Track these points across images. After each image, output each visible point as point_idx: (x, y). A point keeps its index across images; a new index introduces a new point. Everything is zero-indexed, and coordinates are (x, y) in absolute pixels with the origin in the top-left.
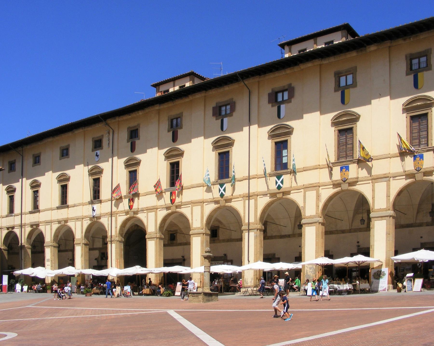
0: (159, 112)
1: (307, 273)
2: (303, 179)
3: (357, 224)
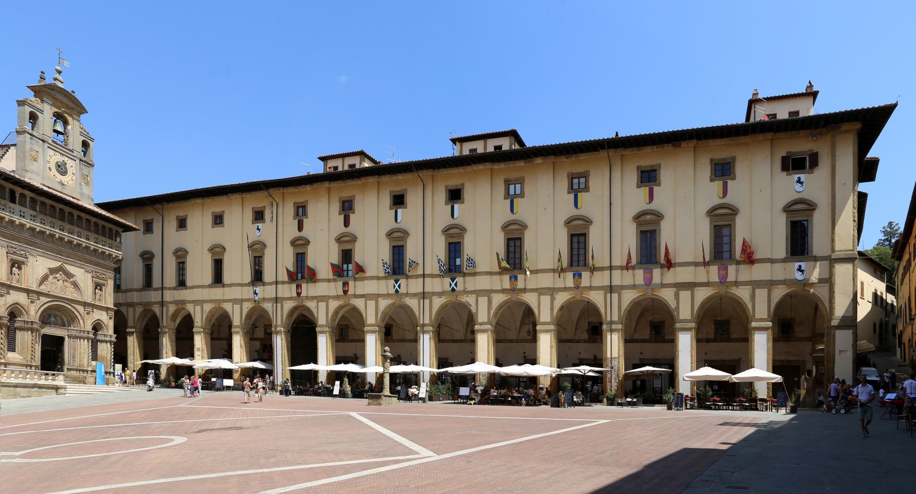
0: (329, 190)
3: (524, 335)
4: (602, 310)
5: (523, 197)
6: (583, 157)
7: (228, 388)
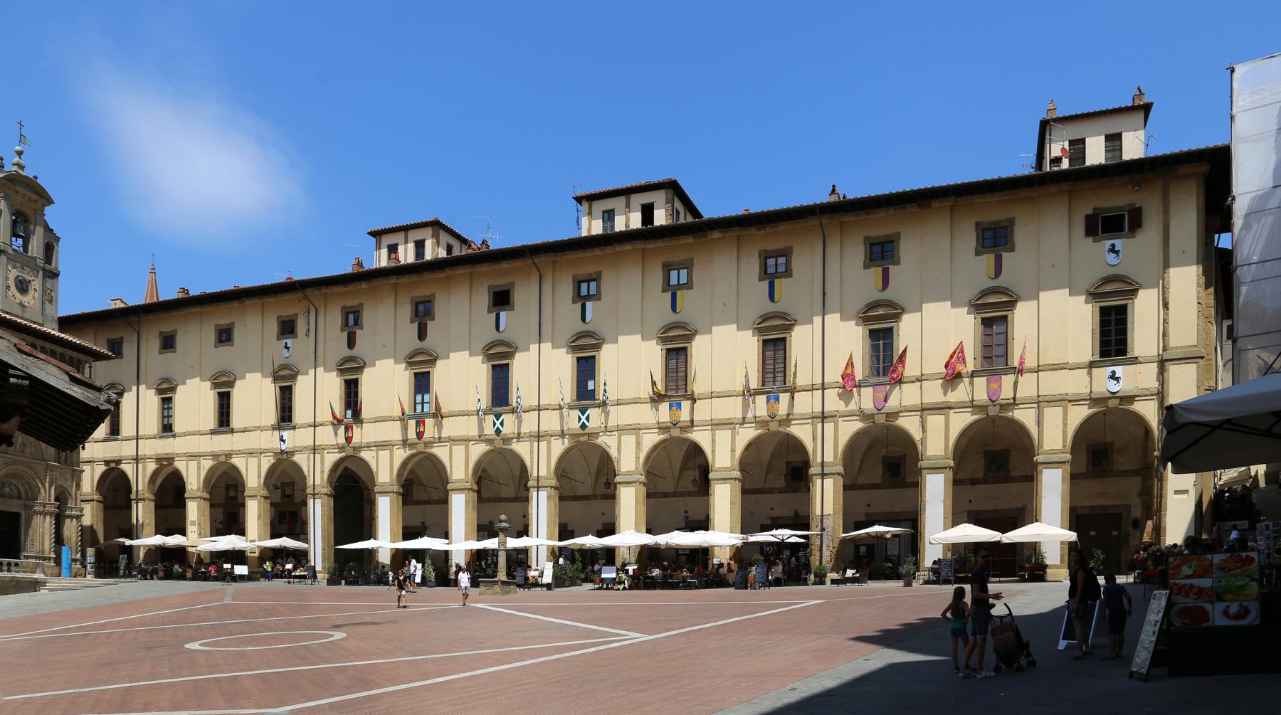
0: (952, 209)
2: (619, 416)
4: (810, 448)
5: (691, 287)
6: (783, 227)
7: (242, 578)
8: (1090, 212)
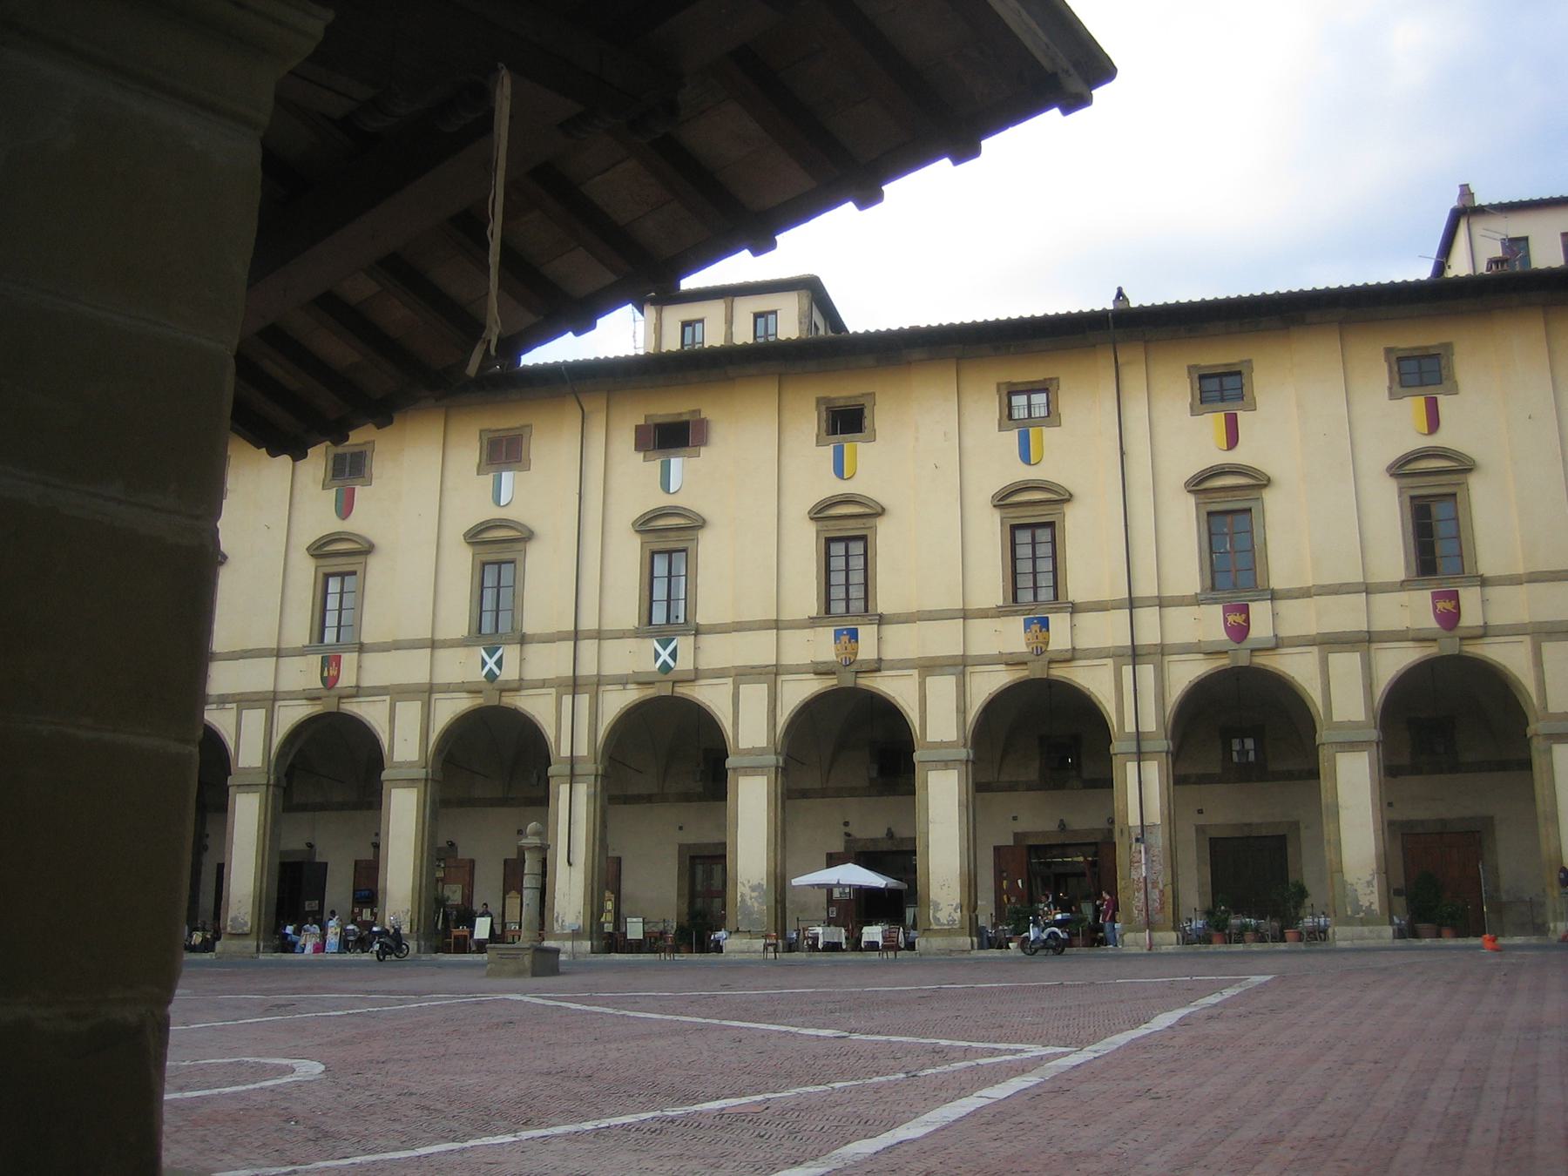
1: (743, 900)
4: (550, 732)
7: (873, 946)
8: (642, 422)
